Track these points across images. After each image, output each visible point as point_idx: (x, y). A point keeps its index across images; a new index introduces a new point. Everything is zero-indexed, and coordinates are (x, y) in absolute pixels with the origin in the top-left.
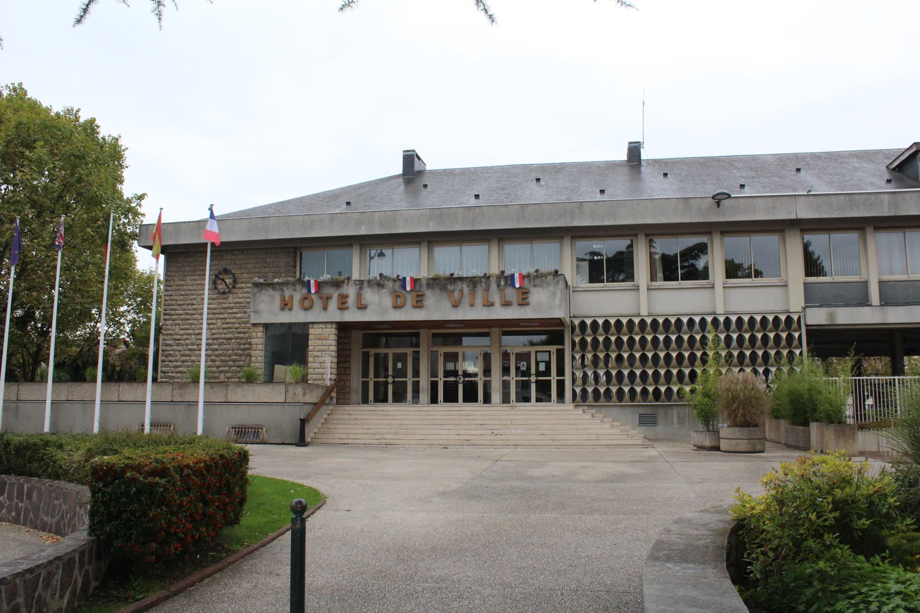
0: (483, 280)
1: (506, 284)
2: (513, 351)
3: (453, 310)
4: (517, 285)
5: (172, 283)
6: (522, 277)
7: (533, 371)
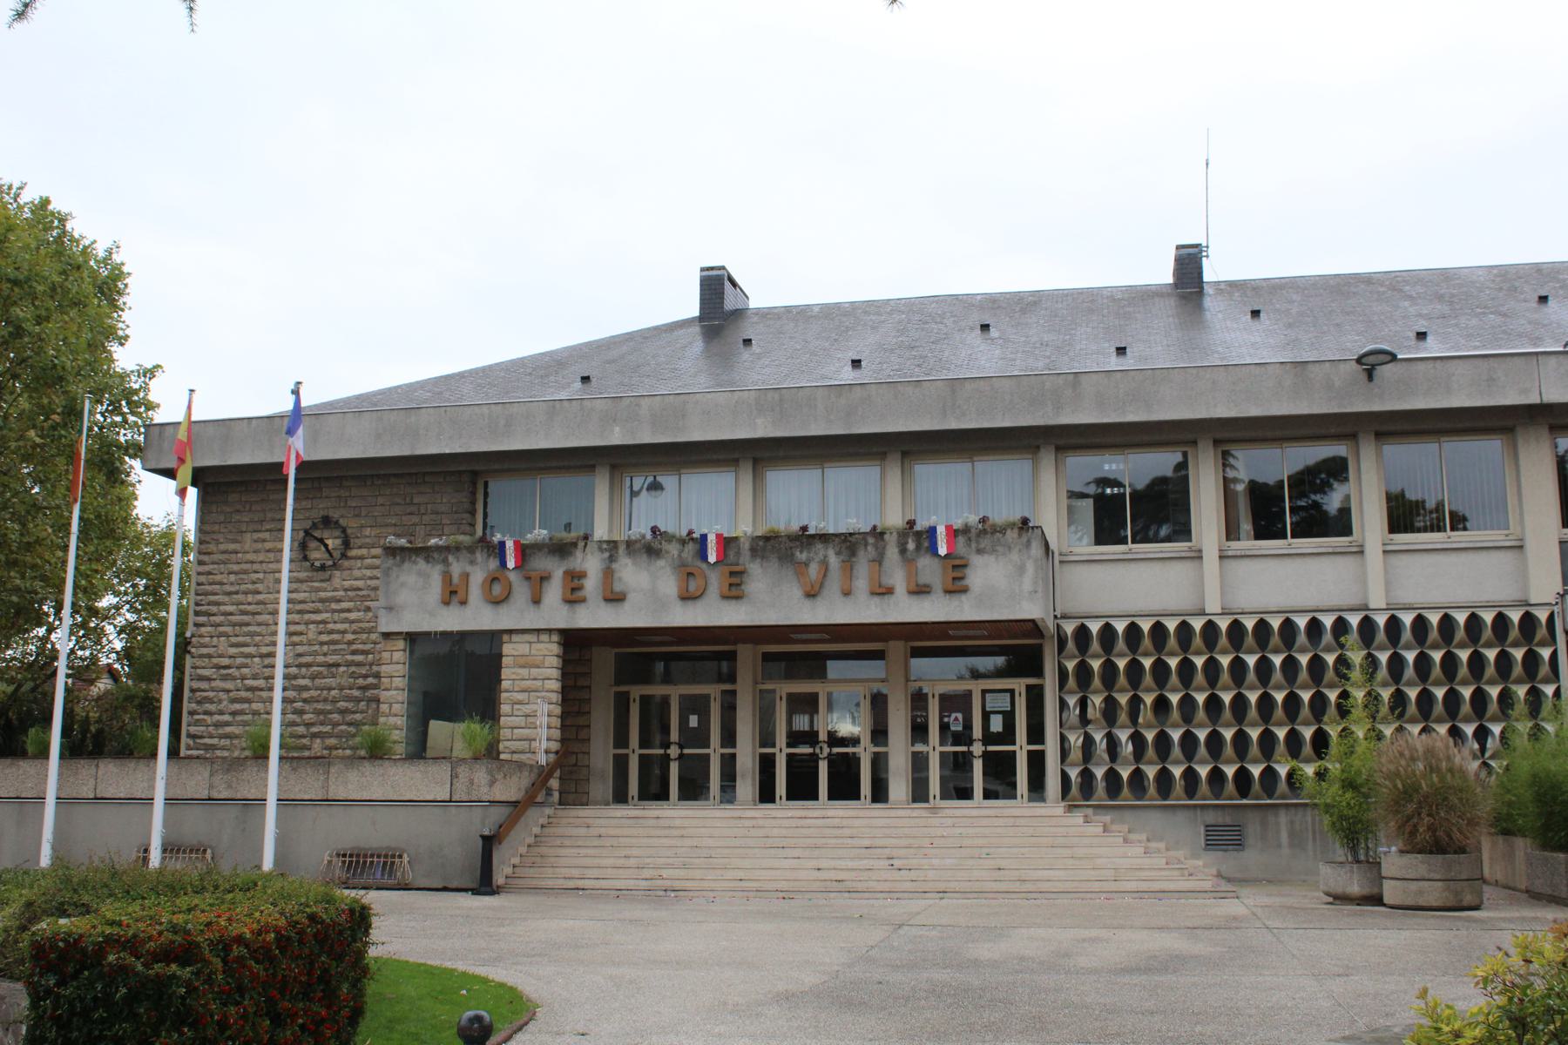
0: (871, 540)
1: (918, 548)
2: (934, 690)
3: (808, 603)
4: (943, 551)
5: (212, 547)
6: (952, 533)
7: (977, 732)
